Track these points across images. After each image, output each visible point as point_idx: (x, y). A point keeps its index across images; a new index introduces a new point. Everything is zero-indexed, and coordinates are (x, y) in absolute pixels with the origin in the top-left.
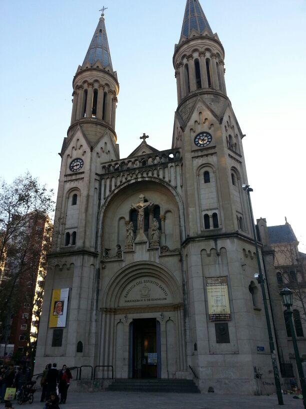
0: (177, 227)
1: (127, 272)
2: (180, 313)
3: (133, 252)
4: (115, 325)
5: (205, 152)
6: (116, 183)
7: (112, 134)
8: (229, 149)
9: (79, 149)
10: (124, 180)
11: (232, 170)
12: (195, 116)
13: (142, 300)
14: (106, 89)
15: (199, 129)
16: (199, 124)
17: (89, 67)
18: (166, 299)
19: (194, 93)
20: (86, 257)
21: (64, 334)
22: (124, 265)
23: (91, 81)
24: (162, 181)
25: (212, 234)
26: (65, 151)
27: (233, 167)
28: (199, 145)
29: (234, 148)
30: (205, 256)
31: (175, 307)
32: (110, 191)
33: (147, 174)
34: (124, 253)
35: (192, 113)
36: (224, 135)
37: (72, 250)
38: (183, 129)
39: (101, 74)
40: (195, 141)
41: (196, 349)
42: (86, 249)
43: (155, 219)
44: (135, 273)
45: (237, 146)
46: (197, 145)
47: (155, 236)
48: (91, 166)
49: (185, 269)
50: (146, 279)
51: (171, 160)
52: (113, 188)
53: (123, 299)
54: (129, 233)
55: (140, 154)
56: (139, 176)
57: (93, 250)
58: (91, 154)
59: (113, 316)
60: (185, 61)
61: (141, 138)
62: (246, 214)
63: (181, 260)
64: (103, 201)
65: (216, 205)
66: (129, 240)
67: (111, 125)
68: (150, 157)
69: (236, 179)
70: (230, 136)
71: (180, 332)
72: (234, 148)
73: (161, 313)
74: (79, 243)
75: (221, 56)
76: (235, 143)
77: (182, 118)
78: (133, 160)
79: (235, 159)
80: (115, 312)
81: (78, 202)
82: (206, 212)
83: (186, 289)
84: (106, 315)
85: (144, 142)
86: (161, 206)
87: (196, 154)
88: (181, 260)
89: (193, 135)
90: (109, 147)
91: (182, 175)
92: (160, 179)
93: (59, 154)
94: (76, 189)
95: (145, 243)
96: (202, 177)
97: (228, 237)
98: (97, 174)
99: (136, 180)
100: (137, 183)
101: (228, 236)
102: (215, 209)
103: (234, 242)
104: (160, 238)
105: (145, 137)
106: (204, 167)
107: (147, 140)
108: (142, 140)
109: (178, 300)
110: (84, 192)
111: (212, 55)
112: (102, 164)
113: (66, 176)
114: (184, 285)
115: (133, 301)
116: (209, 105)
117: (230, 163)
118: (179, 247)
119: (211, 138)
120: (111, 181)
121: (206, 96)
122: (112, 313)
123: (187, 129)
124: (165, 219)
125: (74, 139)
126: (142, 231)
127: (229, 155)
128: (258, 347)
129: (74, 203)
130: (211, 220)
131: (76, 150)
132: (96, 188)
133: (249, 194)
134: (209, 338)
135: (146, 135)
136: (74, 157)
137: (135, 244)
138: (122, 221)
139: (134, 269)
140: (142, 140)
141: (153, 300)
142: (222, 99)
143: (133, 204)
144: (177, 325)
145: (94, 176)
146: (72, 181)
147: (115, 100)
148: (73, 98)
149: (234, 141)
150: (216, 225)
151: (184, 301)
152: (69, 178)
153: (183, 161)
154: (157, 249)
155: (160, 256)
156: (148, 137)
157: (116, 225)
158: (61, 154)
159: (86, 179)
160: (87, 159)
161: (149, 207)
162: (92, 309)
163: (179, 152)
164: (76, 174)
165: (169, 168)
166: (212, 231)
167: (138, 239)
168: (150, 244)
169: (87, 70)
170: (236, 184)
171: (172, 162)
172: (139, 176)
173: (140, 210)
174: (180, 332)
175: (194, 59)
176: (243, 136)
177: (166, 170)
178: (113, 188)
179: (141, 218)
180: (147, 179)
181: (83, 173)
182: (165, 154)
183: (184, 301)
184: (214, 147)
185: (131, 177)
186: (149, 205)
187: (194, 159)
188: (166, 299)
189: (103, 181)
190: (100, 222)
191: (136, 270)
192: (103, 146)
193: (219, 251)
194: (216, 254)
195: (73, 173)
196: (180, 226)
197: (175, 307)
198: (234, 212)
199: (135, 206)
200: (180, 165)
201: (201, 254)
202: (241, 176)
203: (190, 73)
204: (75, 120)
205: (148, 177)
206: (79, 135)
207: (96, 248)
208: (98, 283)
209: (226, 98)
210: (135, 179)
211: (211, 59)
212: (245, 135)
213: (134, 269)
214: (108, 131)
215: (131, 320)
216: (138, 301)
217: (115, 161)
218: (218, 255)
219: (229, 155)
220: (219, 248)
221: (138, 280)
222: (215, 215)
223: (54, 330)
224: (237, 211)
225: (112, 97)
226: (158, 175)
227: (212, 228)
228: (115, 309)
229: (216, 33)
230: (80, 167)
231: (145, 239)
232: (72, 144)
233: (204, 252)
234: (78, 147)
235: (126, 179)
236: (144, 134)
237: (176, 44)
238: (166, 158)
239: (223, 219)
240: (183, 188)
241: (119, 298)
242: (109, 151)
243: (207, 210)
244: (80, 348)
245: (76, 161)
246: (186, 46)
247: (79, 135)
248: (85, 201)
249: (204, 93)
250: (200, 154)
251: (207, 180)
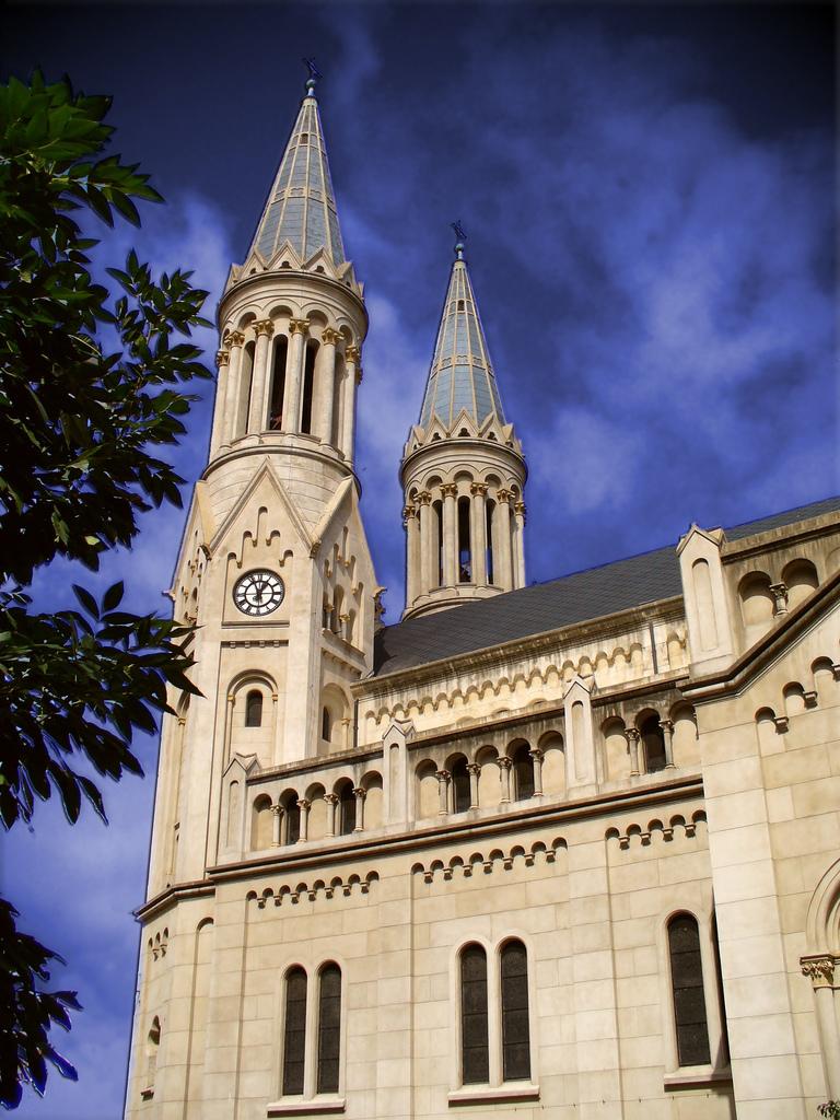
28: (245, 606)
40: (235, 595)
46: (239, 605)
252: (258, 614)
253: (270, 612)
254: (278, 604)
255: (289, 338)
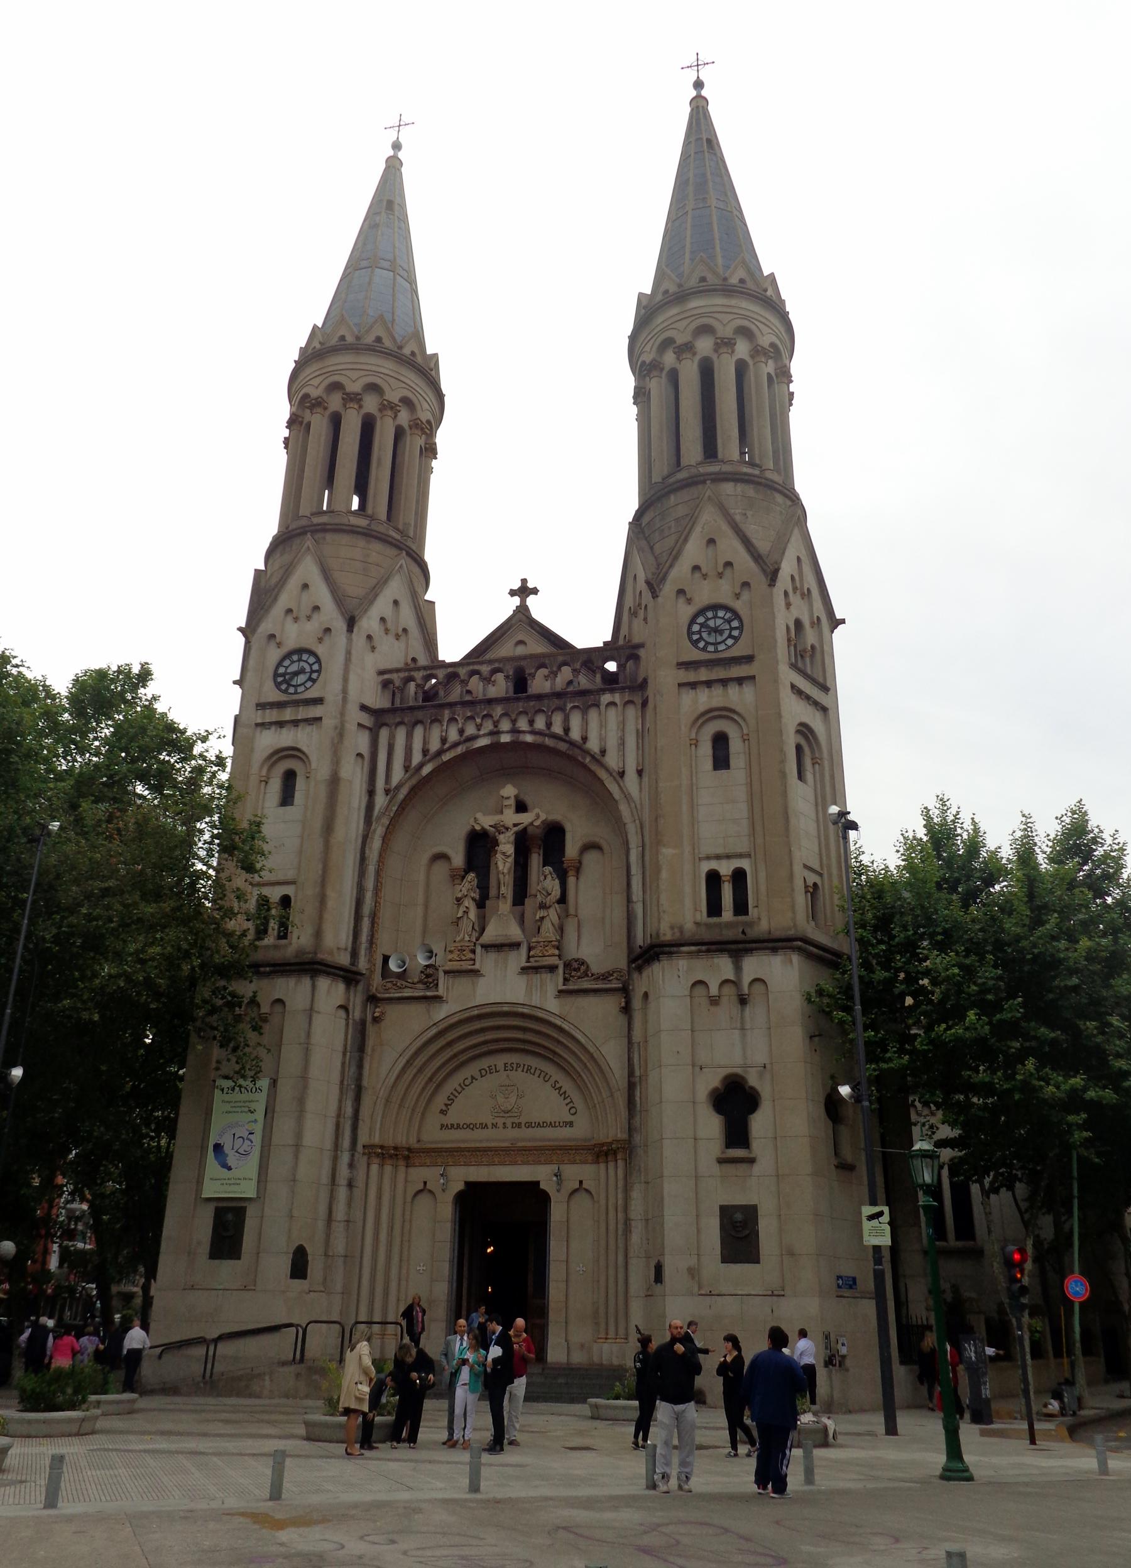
0: (619, 900)
1: (450, 1036)
2: (615, 1171)
3: (475, 973)
4: (409, 1199)
5: (721, 674)
6: (425, 742)
7: (416, 570)
8: (794, 666)
9: (309, 618)
10: (453, 735)
11: (798, 732)
12: (693, 551)
13: (495, 1126)
14: (404, 417)
15: (704, 594)
16: (705, 576)
17: (350, 339)
18: (571, 1124)
19: (694, 471)
20: (323, 983)
21: (250, 1224)
22: (441, 1012)
23: (354, 387)
24: (580, 746)
25: (729, 934)
26: (258, 625)
27: (802, 724)
28: (701, 644)
29: (808, 660)
30: (705, 1002)
31: (603, 1153)
32: (407, 768)
33: (531, 722)
34: (446, 972)
35: (686, 540)
36: (783, 620)
37: (277, 956)
38: (653, 587)
39: (387, 366)
40: (690, 633)
41: (659, 1277)
42: (321, 956)
43: (548, 869)
44: (489, 1036)
45: (818, 656)
46: (695, 643)
47: (547, 926)
48: (346, 680)
49: (637, 1035)
50: (514, 1058)
51: (611, 679)
52: (417, 758)
53: (434, 1120)
54: (462, 909)
55: (506, 650)
56: (505, 725)
57: (344, 960)
58: (350, 641)
59: (402, 1169)
60: (669, 358)
61: (513, 593)
62: (830, 875)
63: (627, 1009)
64: (380, 800)
65: (743, 846)
66: (465, 934)
67: (414, 539)
68: (543, 666)
69: (808, 762)
70: (798, 624)
71: (612, 1227)
72: (808, 660)
73: (555, 1168)
74: (300, 939)
75: (785, 354)
76: (813, 647)
77: (652, 548)
78: (485, 669)
79: (808, 698)
80: (407, 1158)
81: (298, 796)
82: (713, 865)
83: (638, 1099)
84: (382, 1166)
85: (522, 610)
86: (568, 827)
87: (691, 677)
88: (627, 1009)
89: (686, 611)
90: (407, 617)
91: (641, 735)
92: (572, 743)
93: (240, 629)
94: (293, 753)
95: (516, 945)
96: (706, 749)
97: (774, 950)
98: (364, 708)
99: (495, 738)
100: (496, 747)
101: (775, 944)
102: (740, 856)
103: (791, 961)
104: (561, 930)
105: (524, 591)
106: (720, 717)
107: (531, 601)
108: (516, 601)
109: (613, 1130)
110: (321, 768)
111: (757, 352)
112: (381, 673)
113: (261, 706)
114: (631, 1086)
115: (468, 1126)
116: (738, 518)
117: (795, 711)
118: (623, 964)
119: (741, 628)
120: (409, 736)
121: (728, 488)
122: (402, 1163)
123: (668, 589)
124: (578, 871)
125: (294, 583)
126: (505, 906)
127: (793, 686)
128: (839, 1277)
129: (287, 798)
130: (727, 893)
131: (296, 619)
132: (359, 755)
133: (845, 838)
134: (698, 1248)
135: (530, 585)
136: (291, 643)
137: (482, 946)
138: (441, 869)
139: (478, 1025)
140: (516, 601)
141: (529, 1125)
142: (779, 498)
143: (479, 816)
144: (603, 1202)
145: (355, 716)
146: (281, 724)
147: (430, 451)
148: (286, 433)
149: (810, 637)
150: (741, 907)
151: (630, 1136)
152: (272, 715)
153: (650, 692)
154: (552, 969)
155: (560, 992)
156: (535, 591)
157: (421, 877)
158: (247, 631)
159: (329, 723)
160: (333, 653)
161: (530, 829)
162: (336, 1146)
163: (636, 658)
164: (297, 703)
165: (603, 707)
166: (729, 925)
167: (491, 934)
168: (530, 949)
169: (342, 347)
170: (809, 776)
171: (612, 691)
172: (505, 725)
173: (502, 838)
174: (612, 1227)
175: (697, 359)
176: (836, 623)
177: (593, 715)
178: (417, 758)
179: (503, 861)
180: (529, 738)
181: (319, 701)
182: (591, 658)
183: (630, 1136)
184: (749, 659)
185: (479, 727)
186: (531, 824)
187: (684, 690)
188: (571, 1124)
189: (384, 733)
190: (371, 869)
191: (483, 1030)
192: (388, 612)
193: (746, 991)
194: (735, 999)
195: (283, 697)
196: (629, 900)
197: (603, 1153)
198: (798, 870)
199: (486, 821)
200: (638, 700)
201: (691, 997)
202: (825, 755)
203: (682, 397)
204: (297, 517)
205: (533, 732)
206: (308, 569)
207: (354, 954)
208: (360, 1066)
209: (794, 500)
210: (491, 733)
211: (750, 362)
212: (843, 621)
213: (478, 1025)
214: (404, 561)
215: (460, 1186)
216: (484, 1126)
217: (425, 668)
218: (743, 1001)
219: (793, 686)
220: (746, 980)
221: (485, 1063)
222: (739, 876)
223: (217, 1209)
224: (806, 867)
225: (420, 441)
226: (567, 730)
227: (727, 914)
228: (409, 1149)
229: (772, 274)
230: (310, 679)
231: (514, 932)
232: (285, 600)
233: (699, 990)
234: (305, 610)
235: (461, 732)
236: (524, 581)
237: (641, 296)
238: (594, 672)
239: (763, 888)
240: (645, 779)
241: (423, 1114)
242: (405, 630)
243: (718, 857)
244: (299, 1267)
245: (295, 658)
246: (674, 311)
247: (308, 569)
248: (322, 792)
249: (720, 478)
250: (704, 675)
251: (721, 761)
252: (716, 651)
253: (729, 647)
254: (736, 639)
255: (343, 413)
